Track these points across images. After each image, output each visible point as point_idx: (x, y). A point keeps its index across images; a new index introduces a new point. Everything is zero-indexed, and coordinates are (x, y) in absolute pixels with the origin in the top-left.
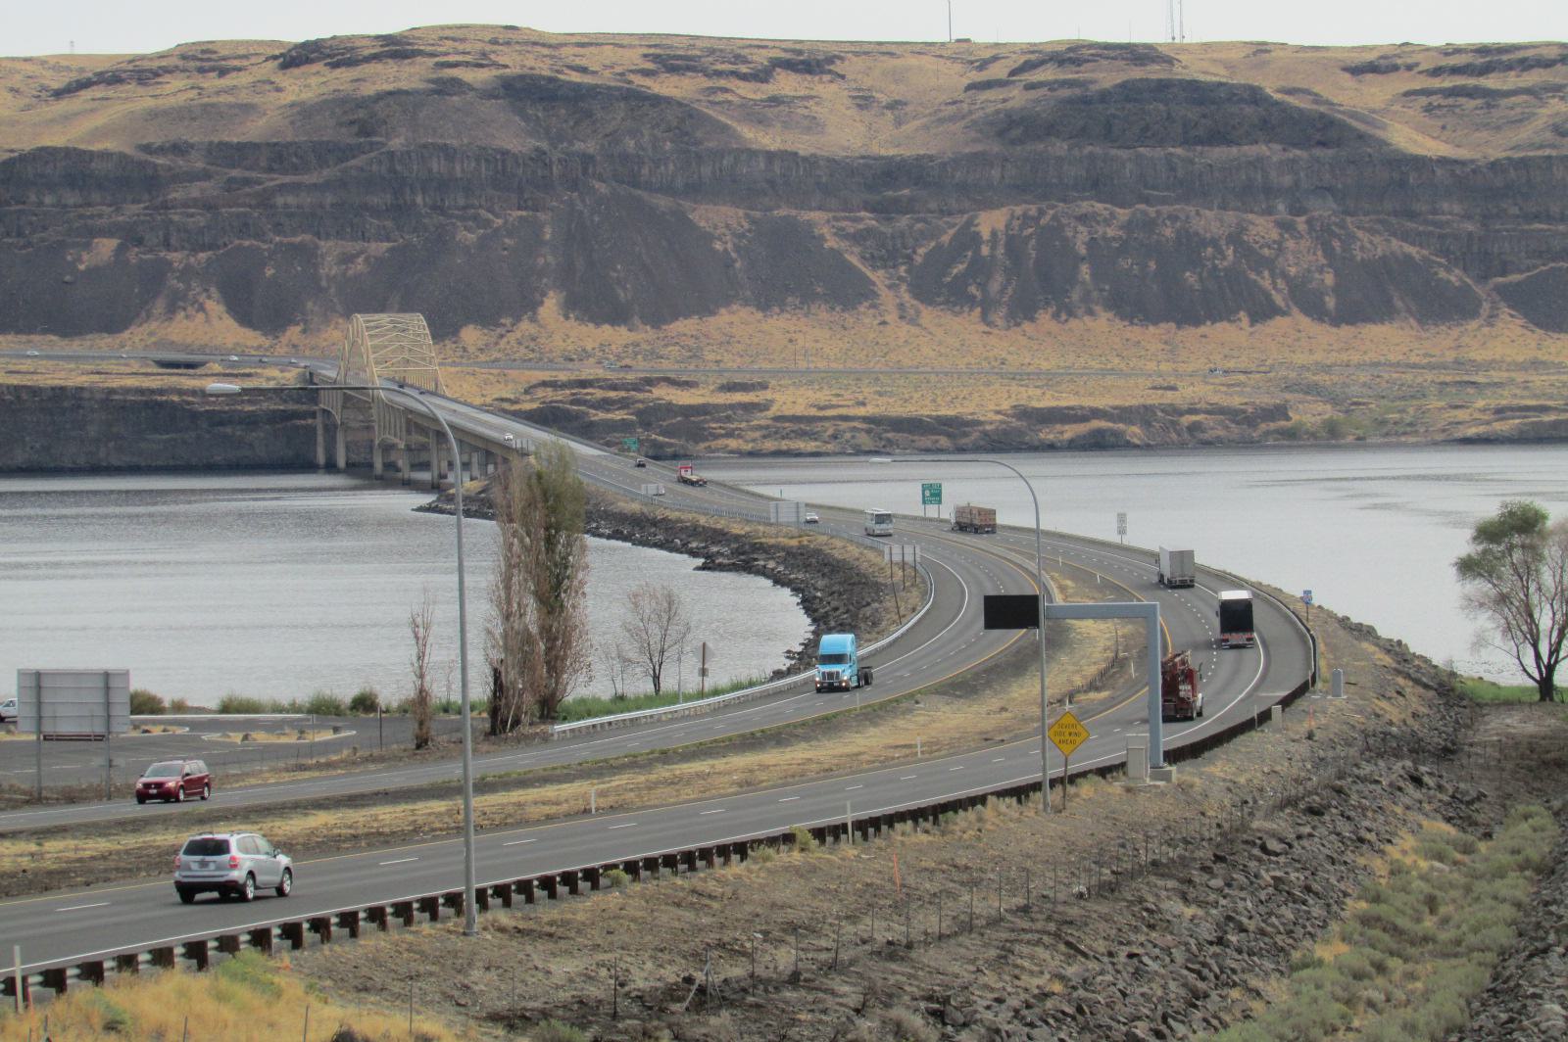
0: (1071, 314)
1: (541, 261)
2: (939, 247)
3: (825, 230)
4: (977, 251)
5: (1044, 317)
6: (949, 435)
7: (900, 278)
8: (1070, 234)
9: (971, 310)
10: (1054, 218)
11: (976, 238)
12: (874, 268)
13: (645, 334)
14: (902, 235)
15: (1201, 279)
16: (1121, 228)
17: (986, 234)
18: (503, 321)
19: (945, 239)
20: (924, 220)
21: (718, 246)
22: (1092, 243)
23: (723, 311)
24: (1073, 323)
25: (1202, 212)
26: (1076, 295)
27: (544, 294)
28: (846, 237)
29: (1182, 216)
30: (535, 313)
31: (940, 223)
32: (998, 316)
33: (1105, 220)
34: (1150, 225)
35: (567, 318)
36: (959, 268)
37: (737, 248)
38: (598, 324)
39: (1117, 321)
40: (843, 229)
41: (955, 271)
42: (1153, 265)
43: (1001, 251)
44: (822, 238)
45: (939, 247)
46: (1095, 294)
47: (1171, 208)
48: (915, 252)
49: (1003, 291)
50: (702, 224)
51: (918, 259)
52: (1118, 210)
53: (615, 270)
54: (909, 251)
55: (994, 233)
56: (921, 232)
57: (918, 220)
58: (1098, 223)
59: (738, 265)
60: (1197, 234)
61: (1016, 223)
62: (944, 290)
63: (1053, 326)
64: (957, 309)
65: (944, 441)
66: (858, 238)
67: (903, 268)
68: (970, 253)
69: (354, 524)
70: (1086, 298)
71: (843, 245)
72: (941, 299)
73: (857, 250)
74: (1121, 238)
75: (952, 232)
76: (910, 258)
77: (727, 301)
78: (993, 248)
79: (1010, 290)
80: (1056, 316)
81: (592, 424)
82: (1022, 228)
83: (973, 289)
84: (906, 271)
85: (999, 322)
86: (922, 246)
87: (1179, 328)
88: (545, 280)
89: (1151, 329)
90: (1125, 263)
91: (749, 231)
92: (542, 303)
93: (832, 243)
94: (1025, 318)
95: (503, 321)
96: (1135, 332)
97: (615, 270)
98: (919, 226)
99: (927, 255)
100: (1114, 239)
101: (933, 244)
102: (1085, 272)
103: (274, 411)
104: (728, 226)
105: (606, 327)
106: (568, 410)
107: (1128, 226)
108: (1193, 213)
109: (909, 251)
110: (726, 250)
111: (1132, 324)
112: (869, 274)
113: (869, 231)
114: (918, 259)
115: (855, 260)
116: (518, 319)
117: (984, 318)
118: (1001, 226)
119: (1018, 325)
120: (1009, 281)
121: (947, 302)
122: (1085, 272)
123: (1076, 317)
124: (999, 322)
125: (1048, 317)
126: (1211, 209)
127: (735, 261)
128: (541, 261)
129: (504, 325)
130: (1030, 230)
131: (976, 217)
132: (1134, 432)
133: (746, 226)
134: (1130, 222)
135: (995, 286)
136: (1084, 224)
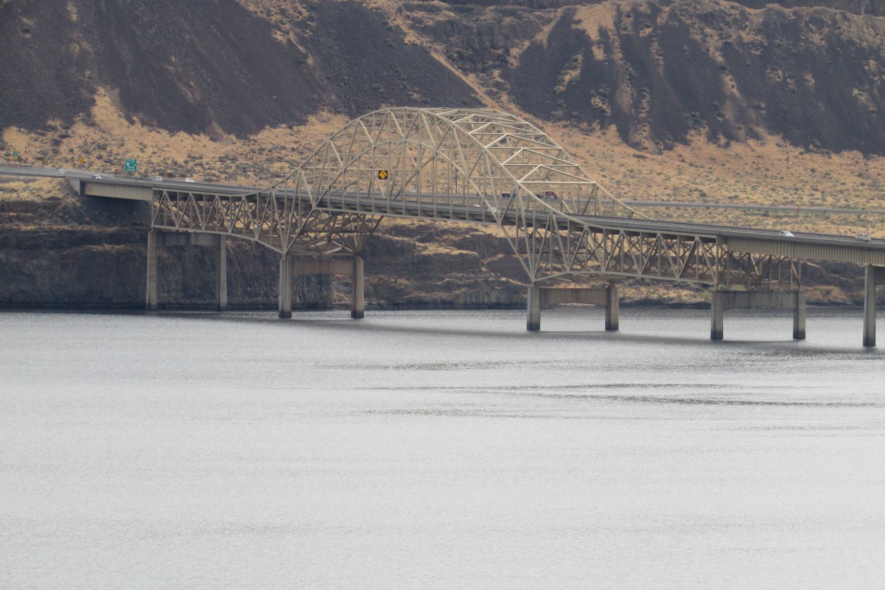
0: (731, 137)
1: (76, 48)
2: (535, 48)
3: (399, 21)
4: (589, 55)
5: (699, 139)
6: (842, 286)
7: (497, 85)
8: (698, 38)
9: (603, 127)
10: (672, 15)
11: (582, 36)
12: (465, 71)
13: (231, 145)
14: (491, 31)
15: (873, 98)
16: (758, 32)
17: (594, 35)
18: (51, 123)
19: (542, 37)
20: (513, 13)
21: (279, 36)
22: (726, 49)
23: (312, 118)
24: (737, 148)
25: (848, 15)
26: (729, 114)
27: (93, 91)
28: (425, 30)
29: (827, 19)
30: (89, 115)
31: (532, 17)
32: (643, 135)
33: (735, 21)
34: (792, 29)
35: (132, 122)
36: (571, 75)
37: (302, 40)
38: (172, 132)
39: (790, 148)
40: (420, 21)
41: (567, 78)
42: (810, 79)
43: (618, 55)
44: (398, 30)
45: (535, 48)
46: (752, 113)
47: (811, 10)
48: (507, 52)
49: (636, 104)
50: (252, 8)
51: (514, 62)
52: (748, 10)
53: (171, 64)
54: (500, 51)
55: (603, 32)
56: (512, 27)
57: (506, 13)
58: (727, 24)
59: (310, 61)
60: (851, 42)
61: (628, 22)
62: (561, 101)
63: (712, 149)
64: (584, 125)
65: (837, 293)
66: (438, 32)
67: (496, 73)
68: (580, 57)
69: (823, 368)
70: (742, 117)
71: (423, 41)
72: (560, 113)
73: (440, 47)
74: (761, 43)
75: (547, 29)
76: (502, 61)
77: (314, 108)
78: (608, 50)
79: (645, 103)
80: (712, 138)
81: (426, 260)
82: (637, 26)
83: (597, 101)
84: (501, 76)
85: (647, 144)
86: (514, 45)
87: (867, 157)
88: (88, 73)
89: (835, 158)
90: (777, 76)
91: (311, 18)
92: (93, 102)
93: (411, 37)
94: (676, 140)
95: (51, 123)
96: (817, 161)
97: (171, 64)
98: (507, 20)
99: (523, 57)
100: (753, 44)
101: (527, 44)
102: (729, 82)
103: (61, 233)
104: (283, 12)
105: (183, 135)
106: (393, 243)
107: (765, 29)
108: (838, 17)
109: (500, 51)
110: (289, 40)
111: (808, 151)
112: (463, 78)
113: (451, 23)
114: (514, 62)
115: (441, 59)
116: (69, 124)
117: (625, 136)
118: (609, 24)
119: (670, 148)
120: (640, 92)
121: (568, 117)
122: (729, 82)
123: (738, 140)
124: (647, 144)
125: (703, 139)
126: (859, 14)
127: (306, 57)
128: (76, 48)
129: (54, 129)
130: (648, 31)
131: (574, 11)
132: (261, 306)
133: (305, 13)
134: (765, 24)
135: (625, 96)
136: (711, 25)
